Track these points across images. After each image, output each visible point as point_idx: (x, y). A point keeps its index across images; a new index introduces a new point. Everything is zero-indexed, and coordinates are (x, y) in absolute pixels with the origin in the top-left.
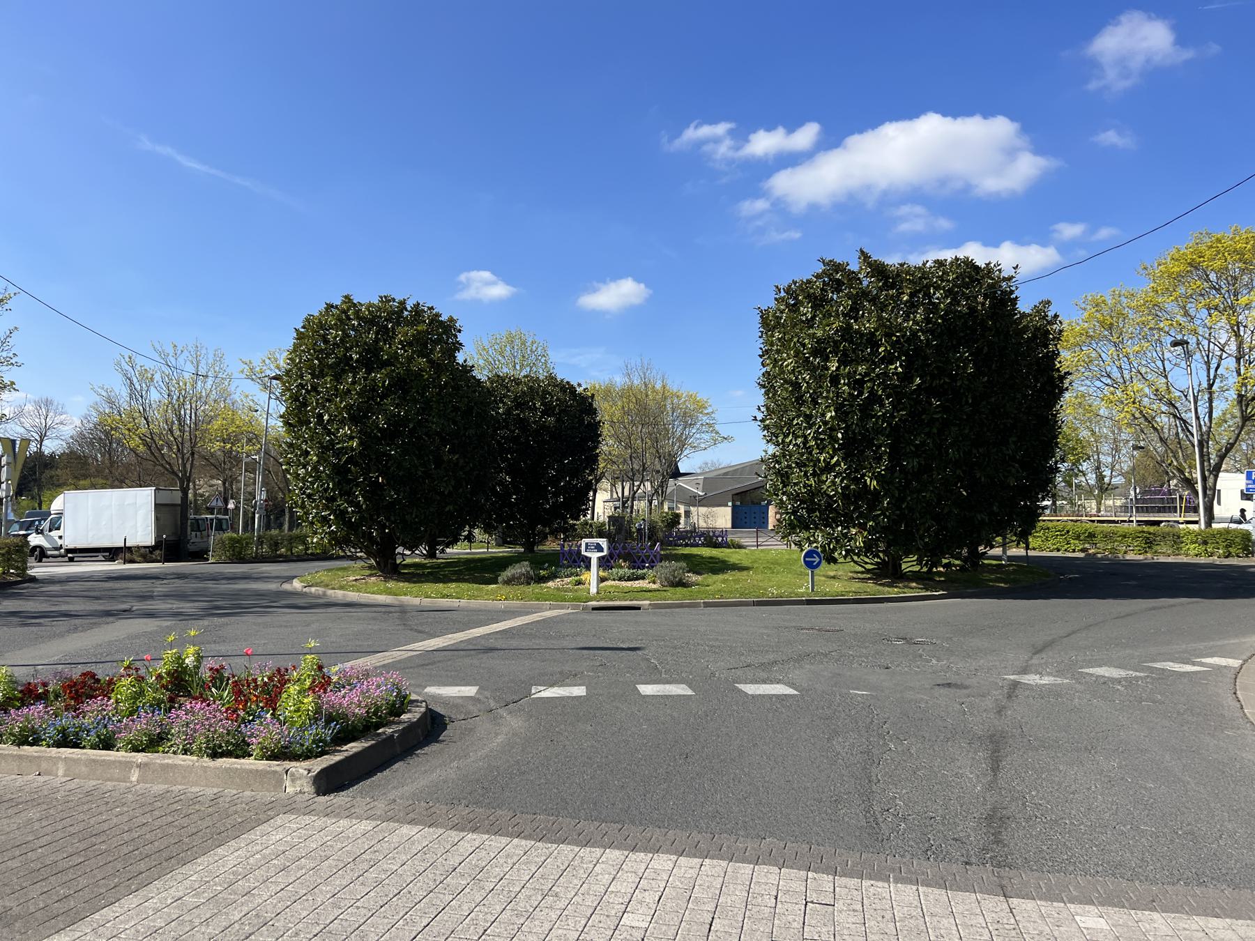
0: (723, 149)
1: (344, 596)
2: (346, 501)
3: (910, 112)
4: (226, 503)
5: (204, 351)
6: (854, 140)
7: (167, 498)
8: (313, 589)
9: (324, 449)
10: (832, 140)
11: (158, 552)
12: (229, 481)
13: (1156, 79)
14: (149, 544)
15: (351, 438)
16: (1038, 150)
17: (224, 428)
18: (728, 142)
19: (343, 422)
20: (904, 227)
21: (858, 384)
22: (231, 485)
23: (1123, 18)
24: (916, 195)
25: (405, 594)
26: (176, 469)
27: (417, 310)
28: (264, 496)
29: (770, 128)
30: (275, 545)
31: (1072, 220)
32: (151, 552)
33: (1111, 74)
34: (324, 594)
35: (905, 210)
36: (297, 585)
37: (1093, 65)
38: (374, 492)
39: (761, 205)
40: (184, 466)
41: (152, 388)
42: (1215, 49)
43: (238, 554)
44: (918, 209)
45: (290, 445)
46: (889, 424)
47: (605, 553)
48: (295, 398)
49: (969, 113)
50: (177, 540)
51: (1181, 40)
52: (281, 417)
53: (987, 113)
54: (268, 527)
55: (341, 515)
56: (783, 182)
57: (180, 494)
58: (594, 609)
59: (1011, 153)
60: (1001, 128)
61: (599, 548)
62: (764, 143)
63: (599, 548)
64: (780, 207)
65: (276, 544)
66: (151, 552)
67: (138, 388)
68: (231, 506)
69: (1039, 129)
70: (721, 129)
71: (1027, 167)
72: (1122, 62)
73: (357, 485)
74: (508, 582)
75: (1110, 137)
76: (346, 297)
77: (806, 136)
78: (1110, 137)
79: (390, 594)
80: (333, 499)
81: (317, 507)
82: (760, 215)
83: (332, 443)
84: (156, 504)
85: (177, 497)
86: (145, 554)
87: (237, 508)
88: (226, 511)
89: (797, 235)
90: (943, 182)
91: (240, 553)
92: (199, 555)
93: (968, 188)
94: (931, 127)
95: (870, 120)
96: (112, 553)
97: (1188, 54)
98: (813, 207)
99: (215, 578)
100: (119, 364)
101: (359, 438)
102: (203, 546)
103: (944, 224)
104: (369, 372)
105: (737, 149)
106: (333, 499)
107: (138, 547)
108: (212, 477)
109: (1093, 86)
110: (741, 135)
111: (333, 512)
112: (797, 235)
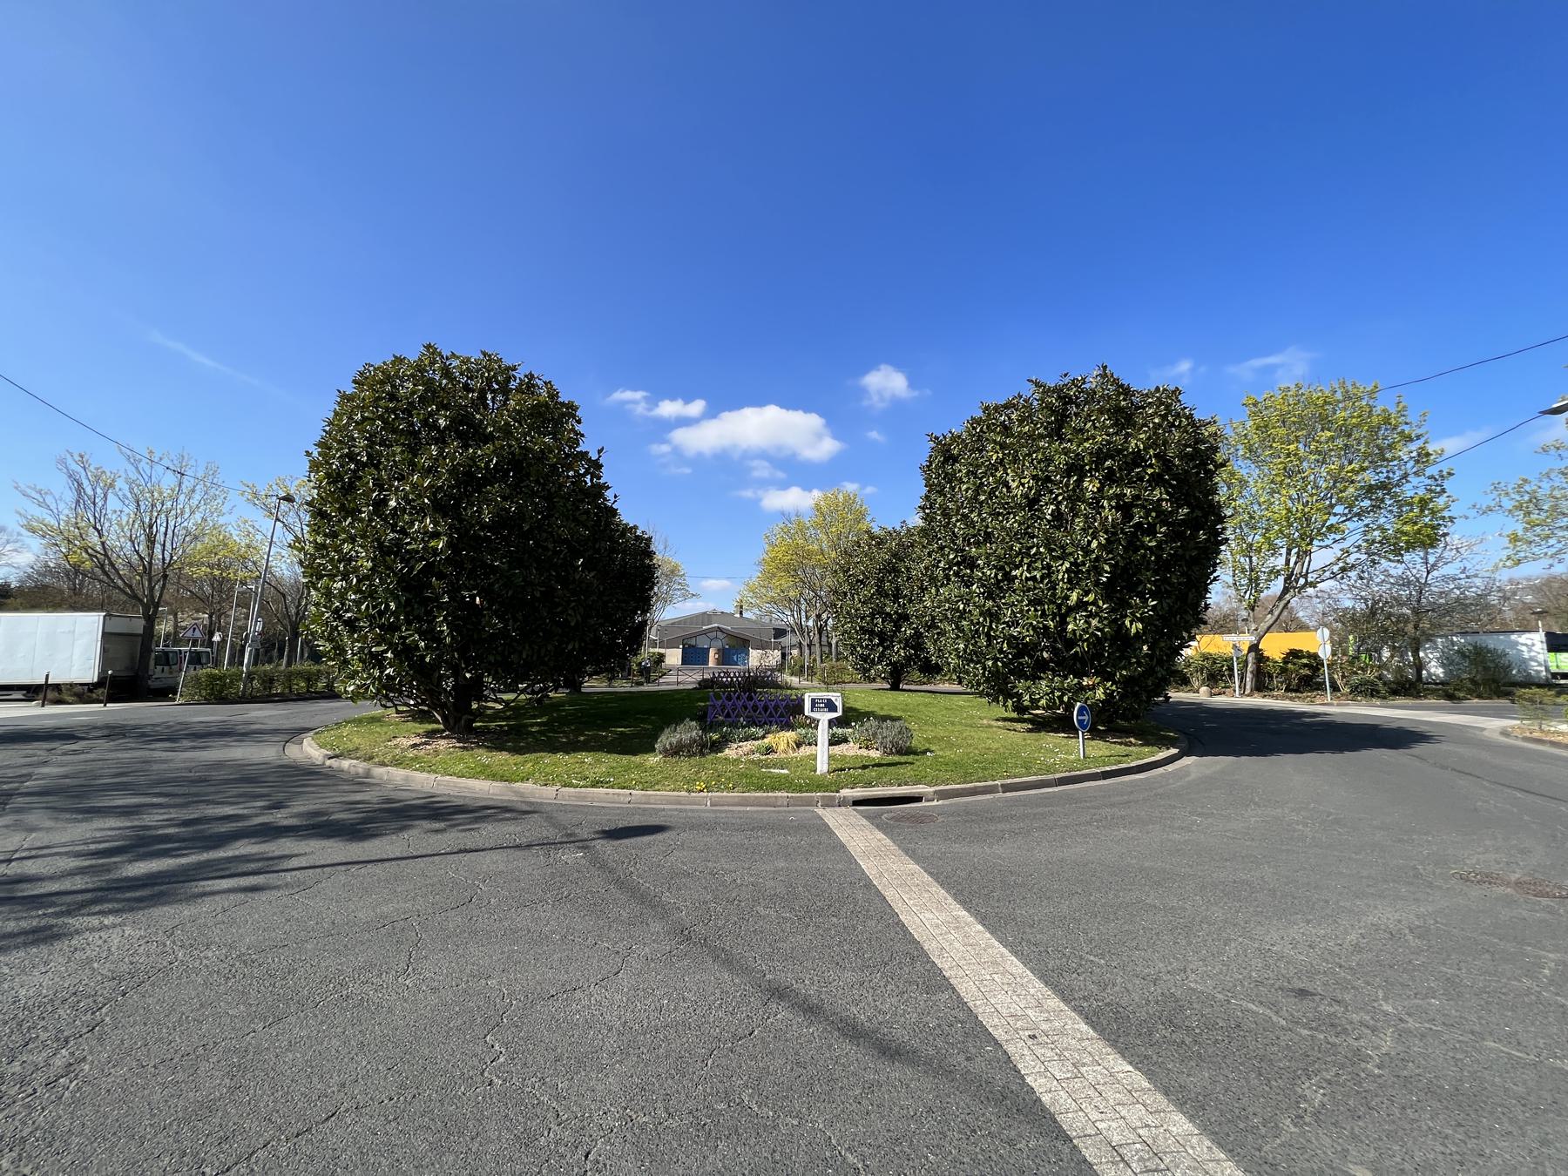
0: (640, 409)
1: (407, 779)
2: (418, 631)
3: (759, 401)
4: (211, 634)
5: (192, 462)
6: (726, 415)
7: (120, 626)
8: (346, 764)
9: (384, 552)
10: (712, 413)
11: (100, 691)
12: (217, 614)
13: (897, 405)
14: (88, 680)
15: (436, 535)
16: (835, 437)
17: (212, 551)
18: (643, 404)
19: (421, 511)
20: (756, 474)
21: (1125, 509)
22: (219, 618)
23: (882, 367)
24: (763, 455)
25: (524, 779)
26: (140, 594)
27: (529, 386)
28: (259, 627)
29: (673, 399)
30: (269, 681)
31: (852, 481)
32: (90, 691)
33: (876, 398)
34: (368, 775)
35: (755, 463)
36: (310, 751)
37: (863, 392)
38: (466, 618)
39: (665, 448)
40: (152, 589)
41: (110, 496)
42: (928, 392)
43: (218, 693)
44: (766, 464)
45: (320, 547)
46: (1159, 557)
47: (839, 713)
48: (334, 477)
49: (795, 409)
50: (130, 674)
51: (912, 384)
52: (309, 504)
53: (807, 410)
54: (255, 664)
55: (405, 653)
56: (681, 436)
57: (143, 622)
58: (857, 803)
59: (819, 437)
60: (813, 421)
61: (831, 706)
62: (669, 409)
63: (831, 706)
64: (677, 452)
65: (271, 681)
66: (90, 691)
67: (90, 492)
68: (216, 638)
69: (837, 423)
70: (639, 395)
71: (828, 447)
72: (879, 392)
73: (441, 607)
74: (675, 751)
75: (874, 435)
76: (428, 347)
77: (696, 408)
78: (874, 435)
79: (494, 777)
80: (393, 628)
81: (363, 639)
82: (663, 455)
83: (398, 543)
84: (104, 634)
85: (138, 626)
86: (83, 693)
87: (224, 641)
88: (211, 644)
89: (688, 471)
90: (779, 448)
91: (221, 692)
92: (164, 693)
93: (794, 455)
94: (772, 412)
95: (736, 404)
96: (32, 692)
97: (916, 393)
98: (700, 455)
99: (172, 735)
100: (63, 461)
101: (450, 536)
102: (170, 682)
103: (781, 475)
104: (466, 447)
105: (650, 410)
106: (393, 628)
107: (72, 685)
108: (198, 611)
109: (865, 403)
110: (653, 401)
111: (391, 646)
112: (688, 471)
